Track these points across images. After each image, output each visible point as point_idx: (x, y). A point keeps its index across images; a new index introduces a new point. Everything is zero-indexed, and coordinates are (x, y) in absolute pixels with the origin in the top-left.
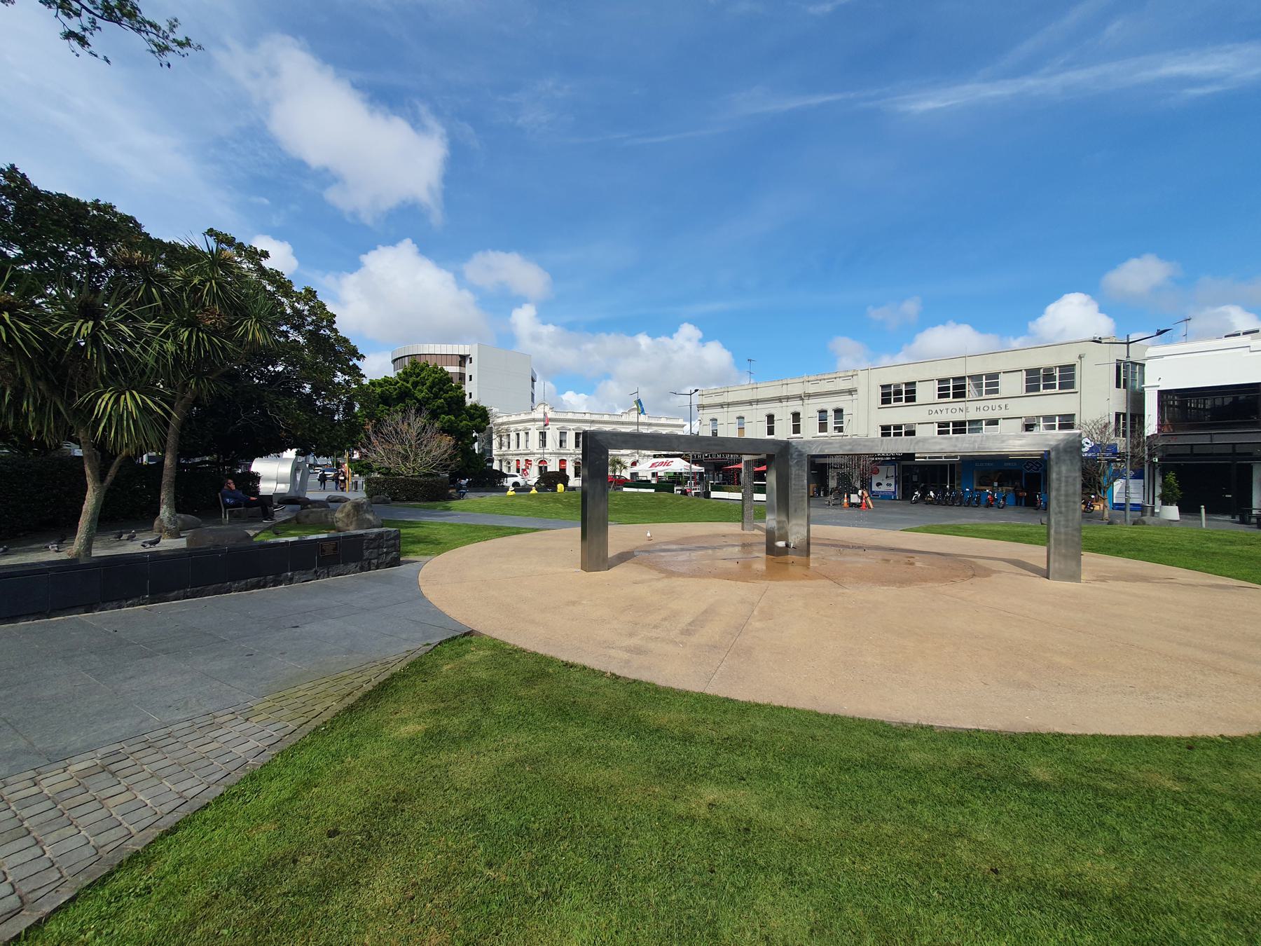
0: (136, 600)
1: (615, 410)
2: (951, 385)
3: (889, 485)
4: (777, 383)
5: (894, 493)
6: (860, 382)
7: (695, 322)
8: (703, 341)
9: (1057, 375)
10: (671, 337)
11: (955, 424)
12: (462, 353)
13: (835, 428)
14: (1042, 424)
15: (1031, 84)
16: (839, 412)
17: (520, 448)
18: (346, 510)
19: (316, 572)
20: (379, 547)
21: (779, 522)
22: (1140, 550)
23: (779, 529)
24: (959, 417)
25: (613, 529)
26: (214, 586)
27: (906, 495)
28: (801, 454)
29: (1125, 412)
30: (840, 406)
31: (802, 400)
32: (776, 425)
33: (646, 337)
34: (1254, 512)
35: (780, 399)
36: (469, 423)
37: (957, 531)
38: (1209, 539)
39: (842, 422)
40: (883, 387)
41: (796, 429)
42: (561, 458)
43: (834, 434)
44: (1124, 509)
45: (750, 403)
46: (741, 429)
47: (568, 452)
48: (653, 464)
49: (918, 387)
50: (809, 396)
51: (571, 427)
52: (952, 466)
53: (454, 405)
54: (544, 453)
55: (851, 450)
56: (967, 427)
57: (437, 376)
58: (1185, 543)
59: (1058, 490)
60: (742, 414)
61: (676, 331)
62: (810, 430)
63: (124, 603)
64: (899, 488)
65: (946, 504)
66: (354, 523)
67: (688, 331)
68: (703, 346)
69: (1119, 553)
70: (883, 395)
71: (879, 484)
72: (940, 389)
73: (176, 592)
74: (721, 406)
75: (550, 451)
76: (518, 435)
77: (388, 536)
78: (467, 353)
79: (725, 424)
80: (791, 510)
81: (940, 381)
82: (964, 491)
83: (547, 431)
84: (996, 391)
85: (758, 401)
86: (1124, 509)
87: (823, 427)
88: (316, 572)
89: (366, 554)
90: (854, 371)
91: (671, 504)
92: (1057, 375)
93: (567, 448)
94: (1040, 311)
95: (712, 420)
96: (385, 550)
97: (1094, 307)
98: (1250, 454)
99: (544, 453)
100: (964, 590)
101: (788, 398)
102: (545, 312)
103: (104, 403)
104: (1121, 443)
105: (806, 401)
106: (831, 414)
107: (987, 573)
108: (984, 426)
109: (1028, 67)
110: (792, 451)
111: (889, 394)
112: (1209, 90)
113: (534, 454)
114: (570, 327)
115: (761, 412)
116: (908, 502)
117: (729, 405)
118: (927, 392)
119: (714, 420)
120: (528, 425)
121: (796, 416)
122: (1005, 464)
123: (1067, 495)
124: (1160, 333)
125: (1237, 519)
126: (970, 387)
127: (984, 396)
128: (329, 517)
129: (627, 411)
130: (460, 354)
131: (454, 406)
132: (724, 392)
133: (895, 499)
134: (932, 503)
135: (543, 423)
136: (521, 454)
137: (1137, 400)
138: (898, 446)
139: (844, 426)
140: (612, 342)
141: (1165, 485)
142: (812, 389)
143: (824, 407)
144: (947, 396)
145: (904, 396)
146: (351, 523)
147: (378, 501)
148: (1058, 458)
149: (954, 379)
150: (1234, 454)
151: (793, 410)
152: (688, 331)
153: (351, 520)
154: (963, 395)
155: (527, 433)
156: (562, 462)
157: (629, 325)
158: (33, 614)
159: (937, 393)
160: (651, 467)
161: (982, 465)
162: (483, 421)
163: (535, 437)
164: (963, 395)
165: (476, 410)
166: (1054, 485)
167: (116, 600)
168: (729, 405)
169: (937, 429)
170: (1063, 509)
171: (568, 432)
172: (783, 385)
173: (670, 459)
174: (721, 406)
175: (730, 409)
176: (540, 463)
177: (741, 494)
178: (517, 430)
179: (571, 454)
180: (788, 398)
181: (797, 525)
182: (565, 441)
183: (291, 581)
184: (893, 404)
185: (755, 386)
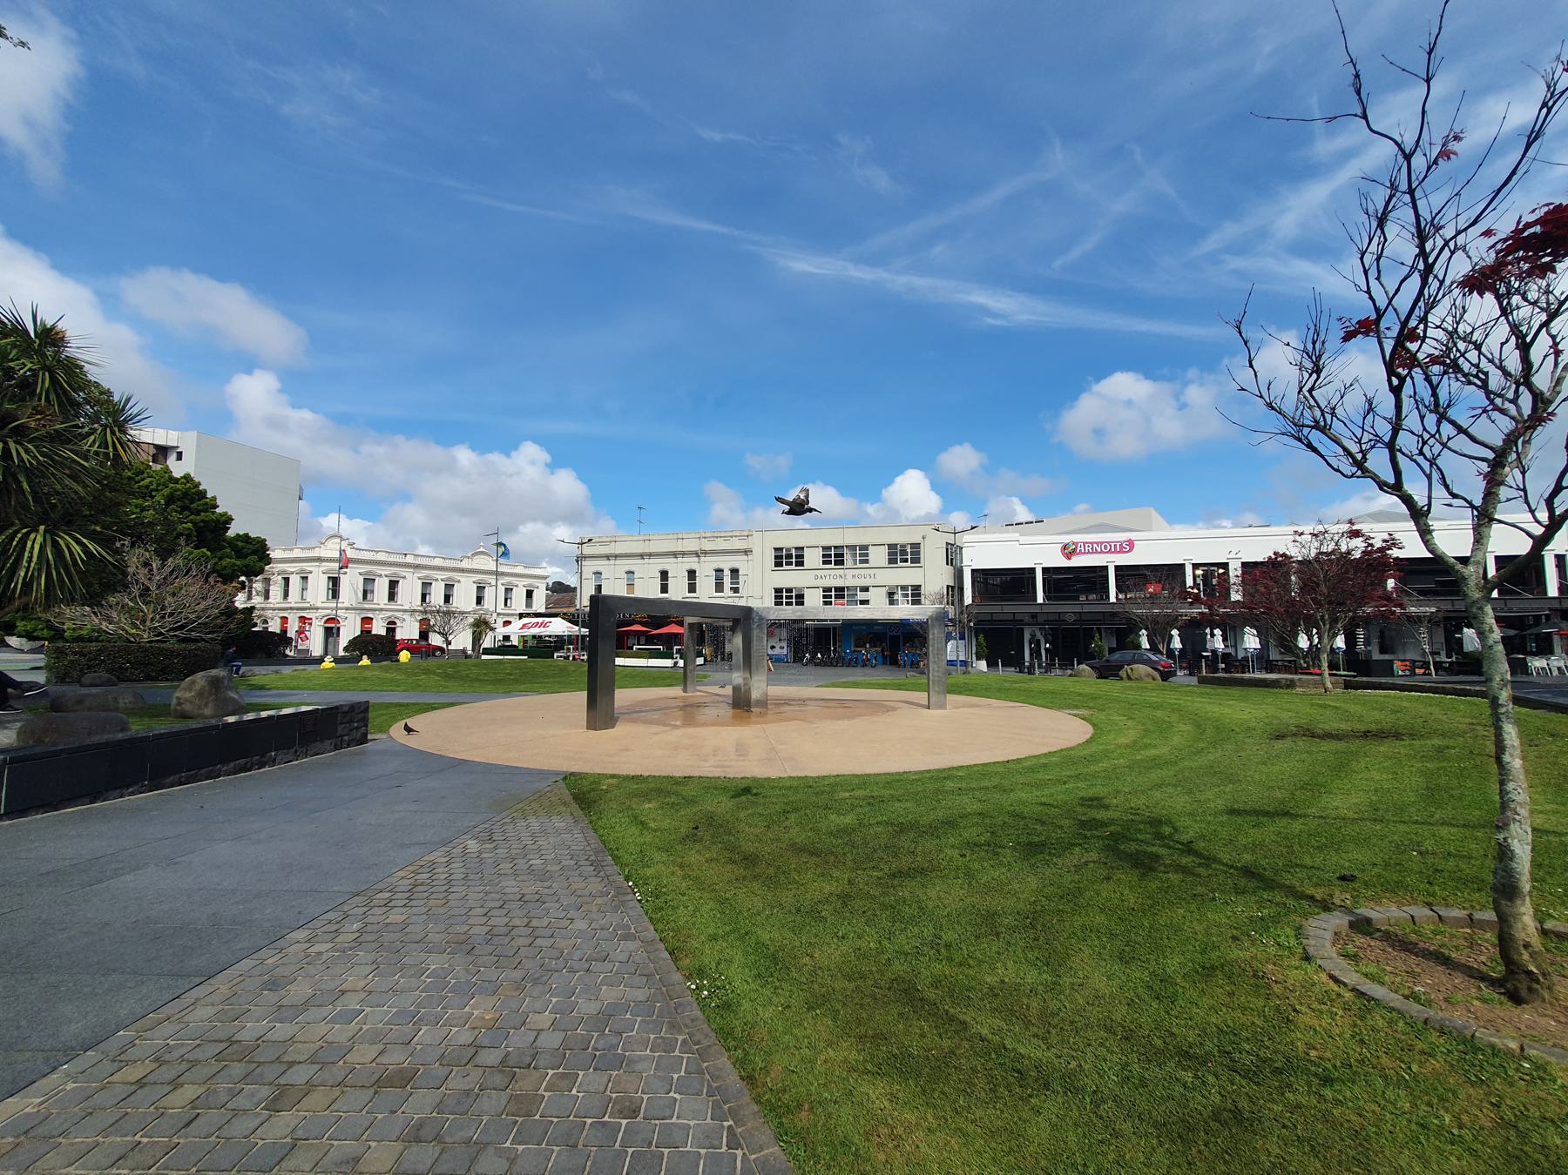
0: (136, 788)
1: (416, 548)
2: (833, 553)
3: (782, 648)
4: (671, 537)
5: (786, 655)
6: (755, 543)
7: (540, 441)
8: (553, 466)
9: (909, 550)
10: (508, 455)
11: (837, 589)
12: (160, 441)
13: (731, 588)
14: (900, 592)
15: (880, 274)
16: (735, 572)
17: (290, 599)
18: (198, 687)
19: (296, 751)
20: (352, 721)
21: (744, 679)
22: (971, 690)
23: (744, 685)
24: (840, 583)
25: (617, 692)
26: (206, 770)
27: (797, 658)
28: (761, 619)
29: (952, 585)
30: (736, 565)
31: (699, 556)
32: (671, 582)
33: (470, 451)
34: (1026, 664)
35: (675, 555)
36: (238, 563)
37: (855, 685)
38: (1005, 681)
39: (738, 583)
40: (776, 549)
41: (692, 588)
42: (505, 620)
43: (730, 595)
44: (956, 665)
45: (642, 556)
46: (631, 585)
47: (400, 608)
48: (524, 625)
49: (806, 552)
50: (705, 553)
51: (439, 577)
52: (835, 628)
53: (208, 534)
54: (337, 609)
55: (801, 616)
56: (846, 593)
57: (179, 486)
58: (993, 684)
59: (933, 646)
60: (632, 569)
61: (516, 449)
62: (706, 593)
63: (125, 791)
64: (791, 651)
65: (831, 665)
66: (210, 705)
67: (531, 455)
68: (553, 473)
69: (960, 693)
70: (776, 557)
71: (773, 647)
72: (824, 556)
73: (172, 778)
74: (608, 557)
75: (347, 605)
76: (287, 580)
77: (359, 708)
78: (171, 443)
79: (612, 578)
80: (753, 668)
81: (824, 548)
82: (846, 653)
83: (341, 576)
84: (867, 561)
85: (650, 555)
86: (956, 665)
87: (719, 587)
88: (296, 751)
89: (340, 728)
90: (749, 531)
91: (574, 671)
92: (909, 550)
93: (399, 603)
94: (890, 482)
95: (595, 573)
96: (356, 725)
97: (926, 483)
98: (1022, 621)
99: (337, 609)
100: (860, 725)
101: (683, 554)
102: (296, 385)
103: (37, 547)
104: (951, 611)
105: (702, 559)
106: (727, 573)
107: (894, 709)
108: (858, 593)
109: (877, 259)
110: (754, 615)
111: (781, 557)
112: (999, 322)
113: (317, 609)
114: (341, 419)
115: (652, 569)
116: (800, 665)
117: (616, 556)
118: (813, 558)
119: (598, 573)
120: (307, 566)
121: (692, 574)
122: (876, 627)
123: (938, 650)
124: (973, 528)
125: (1018, 670)
126: (848, 557)
127: (859, 565)
128: (121, 701)
129: (469, 555)
130: (155, 443)
131: (209, 536)
132: (610, 542)
133: (787, 662)
134: (822, 664)
135: (337, 564)
136: (291, 609)
137: (959, 575)
138: (789, 612)
139: (740, 586)
140: (412, 450)
141: (978, 645)
142: (708, 546)
143: (721, 566)
144: (830, 562)
145: (794, 560)
146: (206, 704)
147: (98, 681)
148: (933, 625)
149: (835, 547)
150: (1014, 620)
151: (688, 567)
152: (531, 455)
153: (205, 700)
154: (842, 563)
155: (305, 579)
156: (284, 620)
157: (445, 432)
158: (69, 800)
159: (821, 559)
160: (521, 628)
161: (857, 628)
162: (261, 559)
163: (319, 584)
164: (842, 563)
165: (247, 543)
166: (931, 643)
167: (119, 788)
168: (616, 556)
169: (822, 593)
170: (936, 659)
171: (377, 579)
172: (678, 539)
173: (547, 619)
174: (608, 557)
175: (617, 562)
176: (326, 622)
177: (1556, 595)
178: (284, 572)
179: (382, 610)
180: (683, 554)
181: (759, 681)
182: (372, 592)
183: (273, 762)
184: (785, 567)
185: (647, 538)
